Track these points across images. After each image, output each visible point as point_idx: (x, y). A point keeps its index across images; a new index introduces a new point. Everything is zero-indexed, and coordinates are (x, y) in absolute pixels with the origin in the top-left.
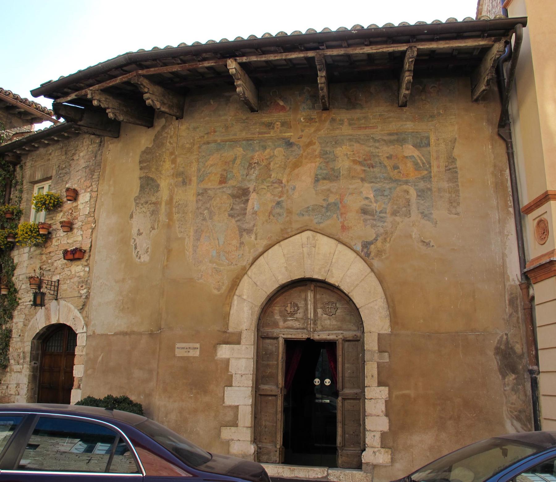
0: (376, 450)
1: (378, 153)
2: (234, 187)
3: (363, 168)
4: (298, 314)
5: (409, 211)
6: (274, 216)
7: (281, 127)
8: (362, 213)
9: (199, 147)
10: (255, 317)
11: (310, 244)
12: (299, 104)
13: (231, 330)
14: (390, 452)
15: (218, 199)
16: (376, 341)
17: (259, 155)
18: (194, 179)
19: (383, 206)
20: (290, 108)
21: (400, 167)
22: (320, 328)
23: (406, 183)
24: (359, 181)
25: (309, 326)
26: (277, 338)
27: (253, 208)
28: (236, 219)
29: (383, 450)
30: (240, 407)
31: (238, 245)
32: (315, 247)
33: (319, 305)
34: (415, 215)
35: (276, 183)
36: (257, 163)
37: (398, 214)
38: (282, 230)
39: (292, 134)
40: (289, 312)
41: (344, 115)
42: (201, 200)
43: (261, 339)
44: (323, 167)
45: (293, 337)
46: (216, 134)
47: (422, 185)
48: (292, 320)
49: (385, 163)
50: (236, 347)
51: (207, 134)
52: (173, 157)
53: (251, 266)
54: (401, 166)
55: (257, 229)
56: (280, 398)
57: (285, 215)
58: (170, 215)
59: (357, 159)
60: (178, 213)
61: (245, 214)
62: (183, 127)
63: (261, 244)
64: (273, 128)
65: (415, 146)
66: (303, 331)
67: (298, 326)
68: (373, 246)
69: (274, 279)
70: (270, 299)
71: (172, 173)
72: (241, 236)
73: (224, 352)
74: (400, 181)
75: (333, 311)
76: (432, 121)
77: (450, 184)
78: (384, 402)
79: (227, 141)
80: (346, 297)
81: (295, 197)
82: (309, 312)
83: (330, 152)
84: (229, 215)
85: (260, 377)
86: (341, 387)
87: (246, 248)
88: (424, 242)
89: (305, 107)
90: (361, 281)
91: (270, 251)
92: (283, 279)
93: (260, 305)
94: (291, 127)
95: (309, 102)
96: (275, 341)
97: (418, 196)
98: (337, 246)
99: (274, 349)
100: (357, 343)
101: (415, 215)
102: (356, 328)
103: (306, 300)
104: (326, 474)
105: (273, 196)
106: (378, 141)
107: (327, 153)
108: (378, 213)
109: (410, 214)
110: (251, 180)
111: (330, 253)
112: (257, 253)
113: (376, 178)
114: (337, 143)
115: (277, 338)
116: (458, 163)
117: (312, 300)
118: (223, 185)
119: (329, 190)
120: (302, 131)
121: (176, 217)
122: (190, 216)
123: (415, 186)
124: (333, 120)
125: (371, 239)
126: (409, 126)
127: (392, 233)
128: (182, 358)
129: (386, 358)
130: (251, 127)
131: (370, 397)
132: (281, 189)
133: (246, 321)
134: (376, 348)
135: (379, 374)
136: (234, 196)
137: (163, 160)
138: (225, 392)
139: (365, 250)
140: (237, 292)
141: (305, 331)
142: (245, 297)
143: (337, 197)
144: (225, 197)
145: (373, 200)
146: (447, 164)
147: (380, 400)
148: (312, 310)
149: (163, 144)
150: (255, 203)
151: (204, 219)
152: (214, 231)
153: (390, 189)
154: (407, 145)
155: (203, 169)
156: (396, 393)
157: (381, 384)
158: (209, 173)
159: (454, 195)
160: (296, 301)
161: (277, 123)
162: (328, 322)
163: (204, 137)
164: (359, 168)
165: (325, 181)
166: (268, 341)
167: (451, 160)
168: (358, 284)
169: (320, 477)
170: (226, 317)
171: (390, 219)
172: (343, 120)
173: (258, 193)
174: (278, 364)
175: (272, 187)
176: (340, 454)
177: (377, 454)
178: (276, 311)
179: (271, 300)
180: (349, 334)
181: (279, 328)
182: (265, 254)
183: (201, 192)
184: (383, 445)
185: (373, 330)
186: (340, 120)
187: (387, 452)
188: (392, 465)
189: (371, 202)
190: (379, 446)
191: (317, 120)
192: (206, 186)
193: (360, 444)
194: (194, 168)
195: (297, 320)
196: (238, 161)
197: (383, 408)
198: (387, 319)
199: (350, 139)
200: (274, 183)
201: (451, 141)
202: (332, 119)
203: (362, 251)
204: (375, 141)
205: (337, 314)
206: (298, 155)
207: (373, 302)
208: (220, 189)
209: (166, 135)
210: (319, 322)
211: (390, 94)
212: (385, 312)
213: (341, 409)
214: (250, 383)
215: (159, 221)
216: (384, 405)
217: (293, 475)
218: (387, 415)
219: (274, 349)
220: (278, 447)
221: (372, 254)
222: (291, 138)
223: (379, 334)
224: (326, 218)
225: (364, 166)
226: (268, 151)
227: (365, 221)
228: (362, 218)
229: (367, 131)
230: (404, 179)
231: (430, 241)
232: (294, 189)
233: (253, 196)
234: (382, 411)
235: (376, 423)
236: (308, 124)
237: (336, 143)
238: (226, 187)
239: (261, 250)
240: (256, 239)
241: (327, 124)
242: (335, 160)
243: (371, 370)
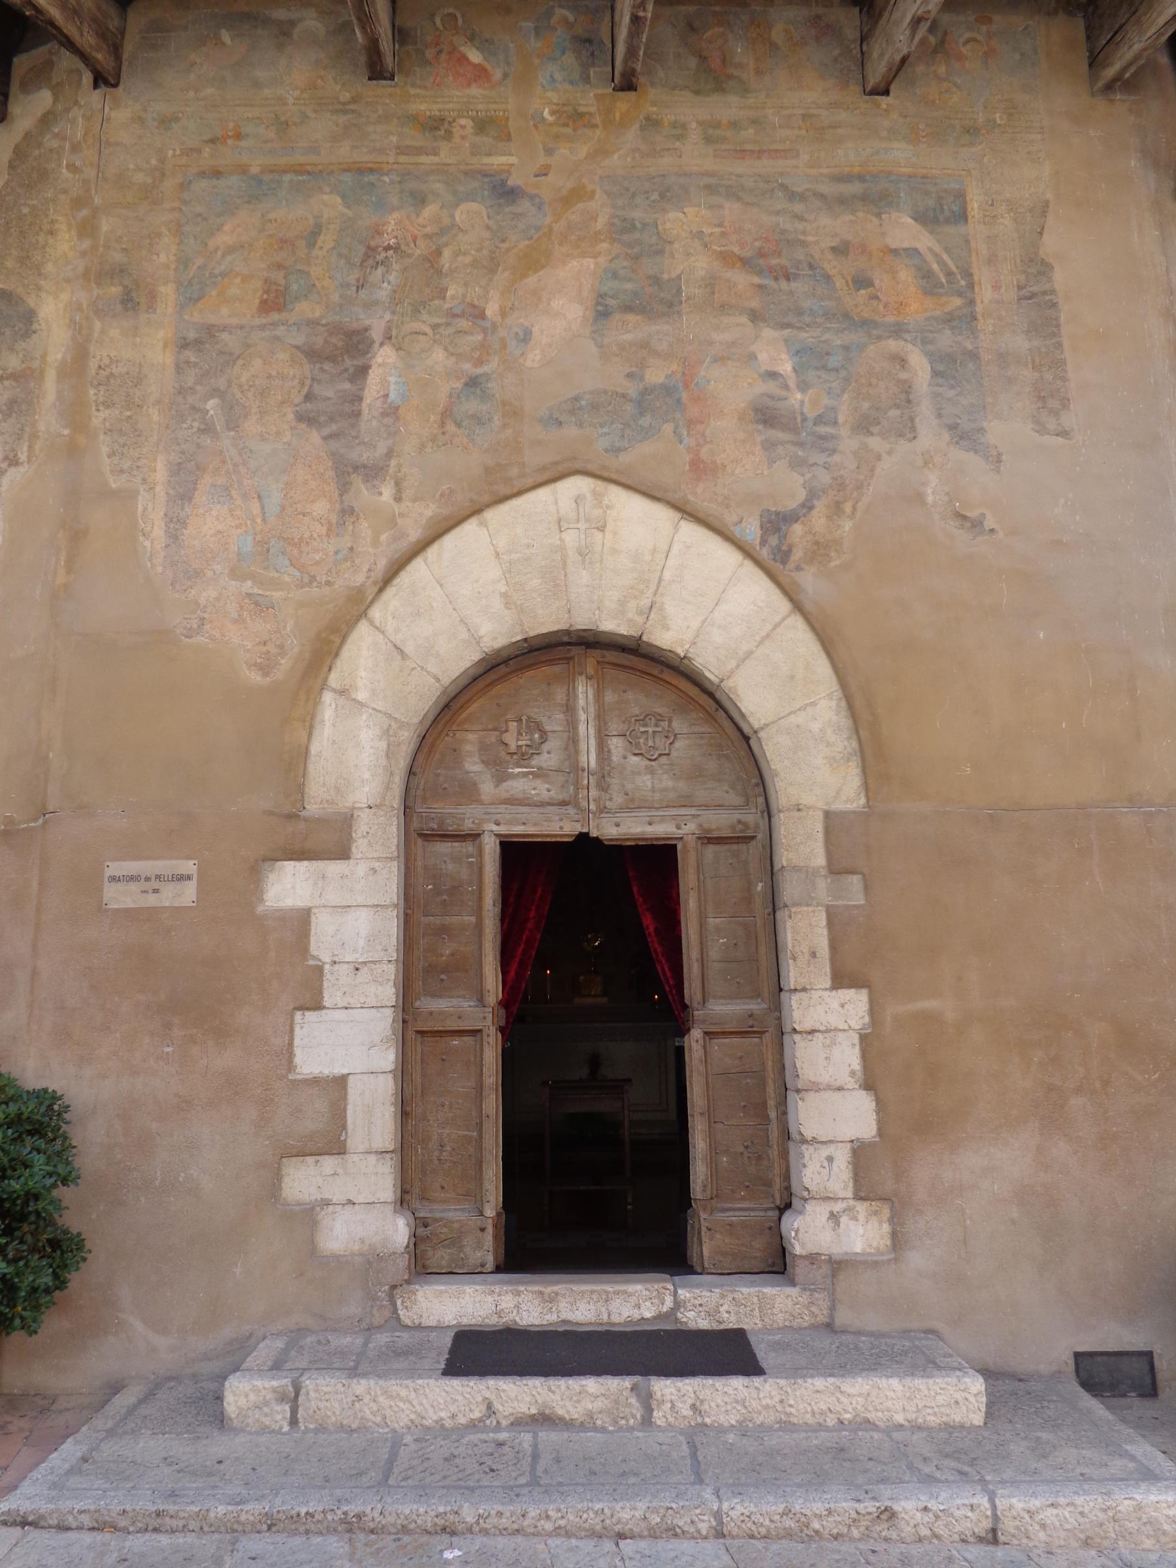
0: (838, 1207)
1: (804, 233)
2: (313, 323)
3: (756, 280)
4: (545, 756)
5: (912, 419)
6: (459, 425)
7: (477, 134)
8: (757, 422)
9: (184, 186)
10: (402, 763)
11: (587, 520)
12: (537, 61)
13: (313, 808)
14: (886, 1212)
15: (257, 362)
16: (820, 837)
17: (399, 223)
18: (168, 292)
19: (826, 401)
20: (505, 75)
21: (877, 282)
22: (619, 799)
23: (898, 331)
24: (744, 319)
25: (582, 794)
26: (475, 836)
27: (386, 396)
28: (326, 431)
29: (862, 1208)
30: (351, 1078)
31: (334, 518)
32: (602, 529)
33: (614, 726)
34: (930, 434)
35: (461, 315)
36: (396, 248)
37: (875, 430)
38: (488, 471)
39: (513, 160)
40: (513, 748)
41: (689, 109)
42: (196, 365)
43: (420, 841)
44: (622, 272)
45: (531, 830)
46: (243, 144)
47: (946, 340)
48: (525, 775)
49: (826, 266)
50: (334, 868)
51: (212, 141)
52: (85, 212)
53: (381, 590)
54: (881, 280)
55: (399, 466)
56: (492, 1040)
57: (497, 420)
58: (75, 414)
59: (736, 250)
60: (108, 405)
61: (358, 414)
62: (121, 115)
63: (415, 518)
64: (449, 136)
65: (921, 218)
66: (563, 810)
67: (545, 796)
68: (798, 529)
69: (464, 635)
70: (447, 706)
71: (81, 269)
72: (344, 487)
73: (289, 886)
74: (876, 324)
75: (661, 744)
76: (971, 144)
77: (1035, 343)
78: (856, 1040)
79: (285, 172)
80: (704, 700)
81: (529, 364)
82: (583, 746)
83: (645, 225)
84: (300, 418)
85: (421, 967)
86: (698, 997)
87: (364, 525)
88: (964, 518)
89: (557, 76)
90: (761, 642)
91: (448, 541)
92: (496, 631)
93: (416, 720)
94: (509, 137)
95: (569, 59)
96: (469, 847)
97: (936, 374)
98: (676, 528)
99: (464, 873)
100: (743, 847)
101: (930, 435)
102: (737, 800)
103: (570, 709)
104: (669, 1302)
105: (453, 359)
106: (802, 197)
107: (634, 227)
108: (810, 424)
109: (913, 429)
110: (377, 303)
111: (654, 551)
112: (404, 545)
113: (800, 312)
114: (668, 195)
115: (475, 836)
116: (1059, 278)
117: (592, 709)
118: (275, 316)
119: (644, 345)
120: (549, 152)
121: (98, 418)
122: (155, 418)
123: (924, 342)
124: (652, 123)
125: (792, 504)
126: (900, 155)
127: (859, 487)
128: (130, 915)
129: (854, 891)
130: (370, 129)
131: (808, 1026)
132: (480, 337)
133: (367, 776)
134: (820, 860)
135: (834, 947)
136: (312, 354)
137: (46, 227)
138: (297, 1030)
139: (774, 541)
140: (334, 680)
141: (571, 810)
142: (362, 696)
143: (674, 367)
144: (283, 356)
145: (792, 384)
146: (1023, 277)
147: (840, 1034)
148: (593, 742)
149: (44, 175)
150: (392, 379)
151: (208, 429)
152: (243, 470)
153: (846, 348)
154: (894, 215)
155: (199, 261)
156: (893, 1009)
157: (840, 980)
158: (223, 275)
159: (1049, 376)
160: (535, 712)
161: (463, 122)
162: (645, 781)
163: (199, 151)
164: (742, 280)
165: (631, 317)
166: (444, 847)
167: (1036, 266)
168: (752, 652)
169: (648, 1315)
170: (294, 763)
171: (849, 443)
172: (684, 126)
173: (399, 349)
174: (479, 926)
175: (450, 330)
176: (704, 1224)
177: (844, 1220)
178: (468, 747)
179: (451, 709)
180: (720, 821)
181: (479, 802)
182: (432, 552)
183: (192, 335)
184: (864, 1189)
185: (807, 799)
186: (674, 125)
187: (876, 1213)
188: (896, 1260)
189: (786, 387)
190: (850, 1194)
191: (598, 120)
192: (212, 319)
193: (769, 1184)
194: (165, 254)
195: (540, 774)
196: (326, 240)
197: (856, 1063)
198: (853, 764)
199: (708, 187)
200: (455, 316)
201: (1031, 211)
202: (648, 119)
203: (763, 542)
204: (792, 196)
205: (674, 754)
206: (538, 228)
207: (803, 708)
208: (262, 327)
209: (55, 144)
210: (614, 782)
211: (836, 52)
212: (842, 743)
213: (702, 1068)
214: (388, 993)
215: (34, 436)
216: (857, 1050)
217: (553, 1318)
218: (868, 1085)
219: (464, 873)
220: (490, 1212)
221: (797, 555)
222: (509, 172)
223: (828, 815)
224: (629, 435)
225: (760, 273)
226: (430, 210)
227: (769, 446)
228: (759, 438)
229: (765, 166)
230: (890, 319)
231: (983, 515)
232: (526, 337)
233: (384, 357)
234: (853, 1073)
235: (834, 1115)
236: (568, 131)
237: (662, 196)
238: (285, 323)
239: (415, 535)
240: (398, 499)
241: (632, 136)
242: (661, 252)
243: (806, 933)
